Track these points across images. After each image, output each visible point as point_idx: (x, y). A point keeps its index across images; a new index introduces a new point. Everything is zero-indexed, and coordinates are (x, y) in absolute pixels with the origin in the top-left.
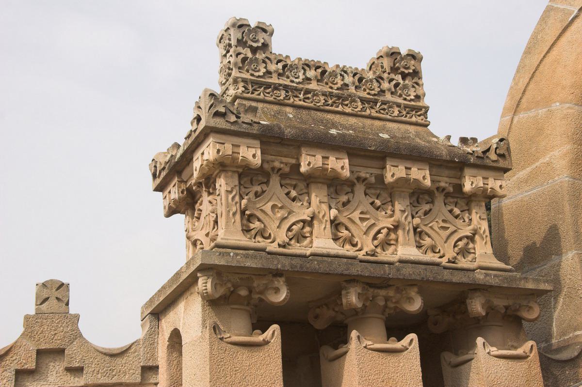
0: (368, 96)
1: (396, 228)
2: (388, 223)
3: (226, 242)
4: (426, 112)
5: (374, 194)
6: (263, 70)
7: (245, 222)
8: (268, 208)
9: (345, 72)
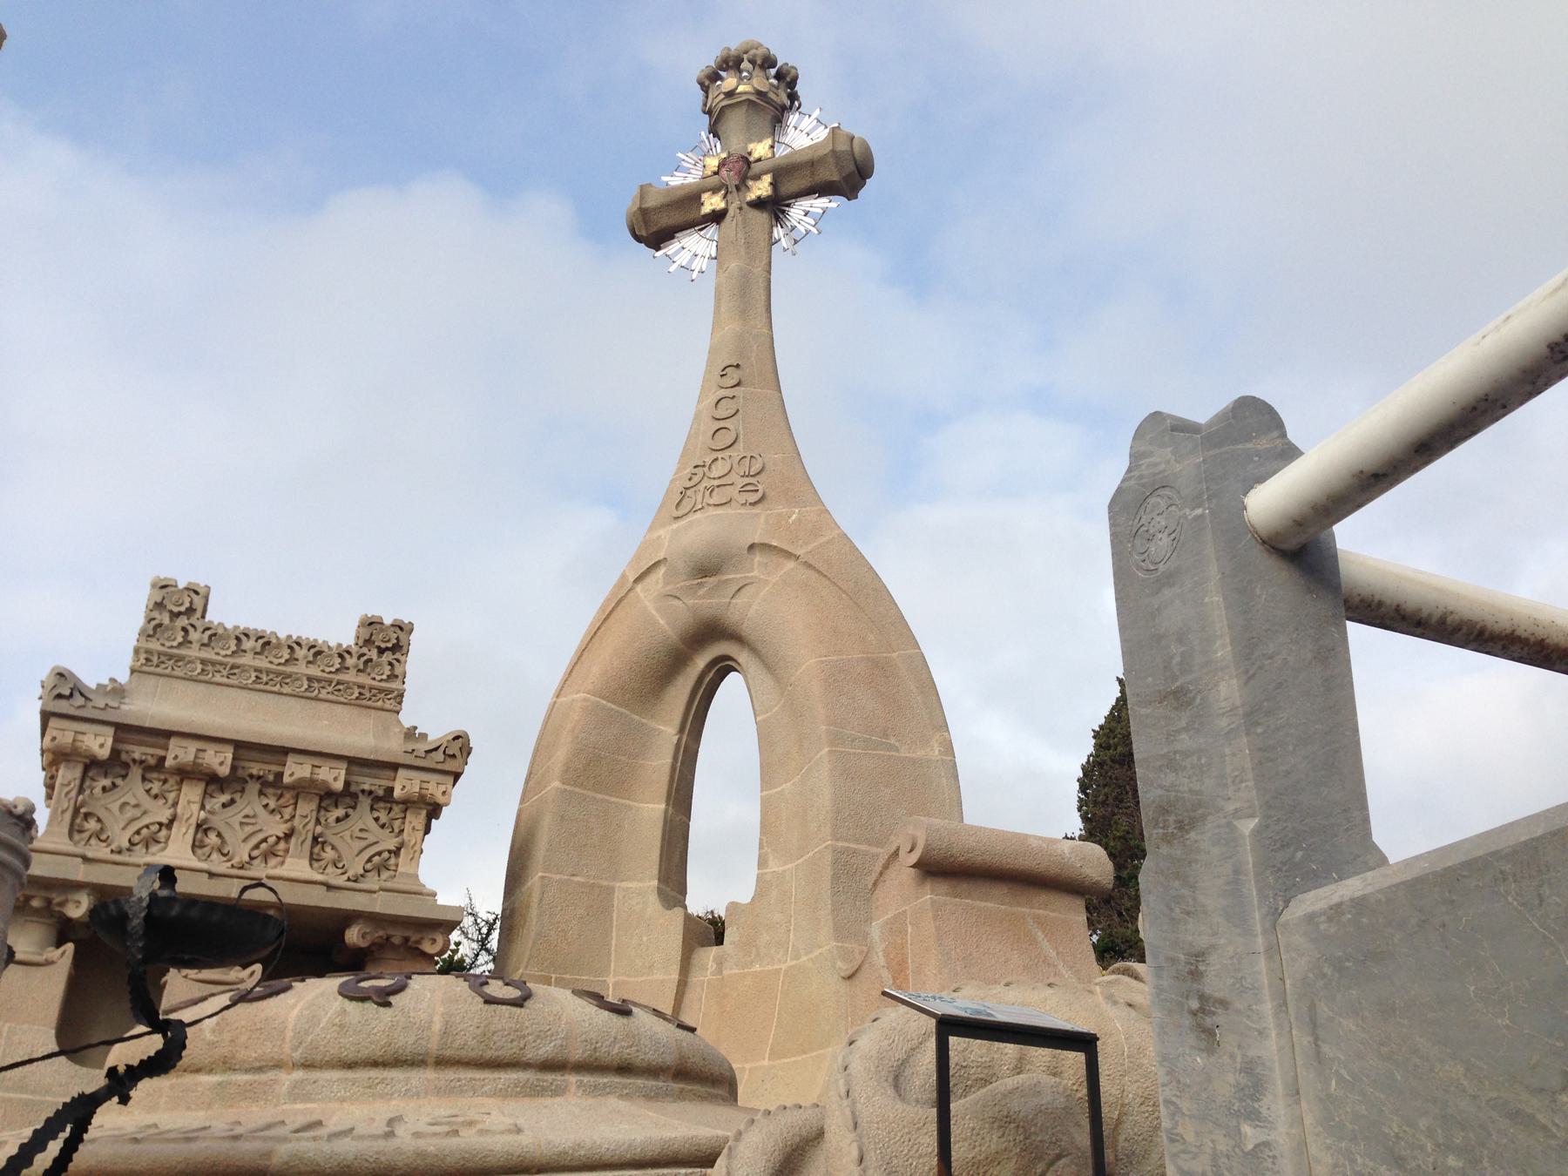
0: (320, 674)
1: (288, 836)
2: (281, 829)
3: (1019, 904)
6: (287, 656)
8: (115, 807)
9: (299, 644)
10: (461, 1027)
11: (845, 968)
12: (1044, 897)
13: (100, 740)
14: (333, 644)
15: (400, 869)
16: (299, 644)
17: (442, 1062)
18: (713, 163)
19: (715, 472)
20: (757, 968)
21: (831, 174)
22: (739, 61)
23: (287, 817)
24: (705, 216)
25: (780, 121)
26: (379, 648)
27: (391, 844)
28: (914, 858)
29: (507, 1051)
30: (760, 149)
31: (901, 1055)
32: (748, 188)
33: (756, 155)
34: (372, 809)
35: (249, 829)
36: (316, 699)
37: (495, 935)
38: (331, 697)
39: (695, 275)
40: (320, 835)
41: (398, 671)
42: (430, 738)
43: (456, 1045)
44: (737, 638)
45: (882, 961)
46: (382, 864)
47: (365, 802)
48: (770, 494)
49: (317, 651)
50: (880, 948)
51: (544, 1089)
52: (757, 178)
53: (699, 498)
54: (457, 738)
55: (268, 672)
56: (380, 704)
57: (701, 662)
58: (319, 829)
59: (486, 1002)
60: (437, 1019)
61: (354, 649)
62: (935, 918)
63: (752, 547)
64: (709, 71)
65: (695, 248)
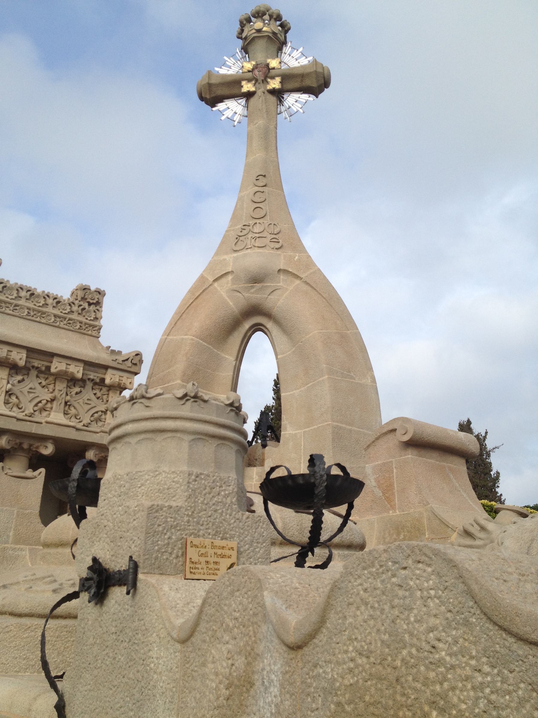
0: (60, 314)
1: (52, 400)
2: (48, 397)
4: (100, 329)
5: (44, 378)
7: (7, 397)
9: (48, 296)
13: (20, 356)
16: (48, 296)
21: (312, 83)
22: (264, 14)
23: (51, 390)
24: (244, 93)
26: (88, 302)
30: (273, 63)
34: (93, 389)
35: (32, 395)
36: (58, 327)
42: (123, 353)
44: (268, 315)
45: (374, 484)
47: (89, 385)
52: (273, 78)
53: (249, 242)
54: (137, 355)
55: (34, 310)
56: (90, 332)
57: (247, 325)
63: (279, 271)
64: (246, 16)
65: (233, 108)
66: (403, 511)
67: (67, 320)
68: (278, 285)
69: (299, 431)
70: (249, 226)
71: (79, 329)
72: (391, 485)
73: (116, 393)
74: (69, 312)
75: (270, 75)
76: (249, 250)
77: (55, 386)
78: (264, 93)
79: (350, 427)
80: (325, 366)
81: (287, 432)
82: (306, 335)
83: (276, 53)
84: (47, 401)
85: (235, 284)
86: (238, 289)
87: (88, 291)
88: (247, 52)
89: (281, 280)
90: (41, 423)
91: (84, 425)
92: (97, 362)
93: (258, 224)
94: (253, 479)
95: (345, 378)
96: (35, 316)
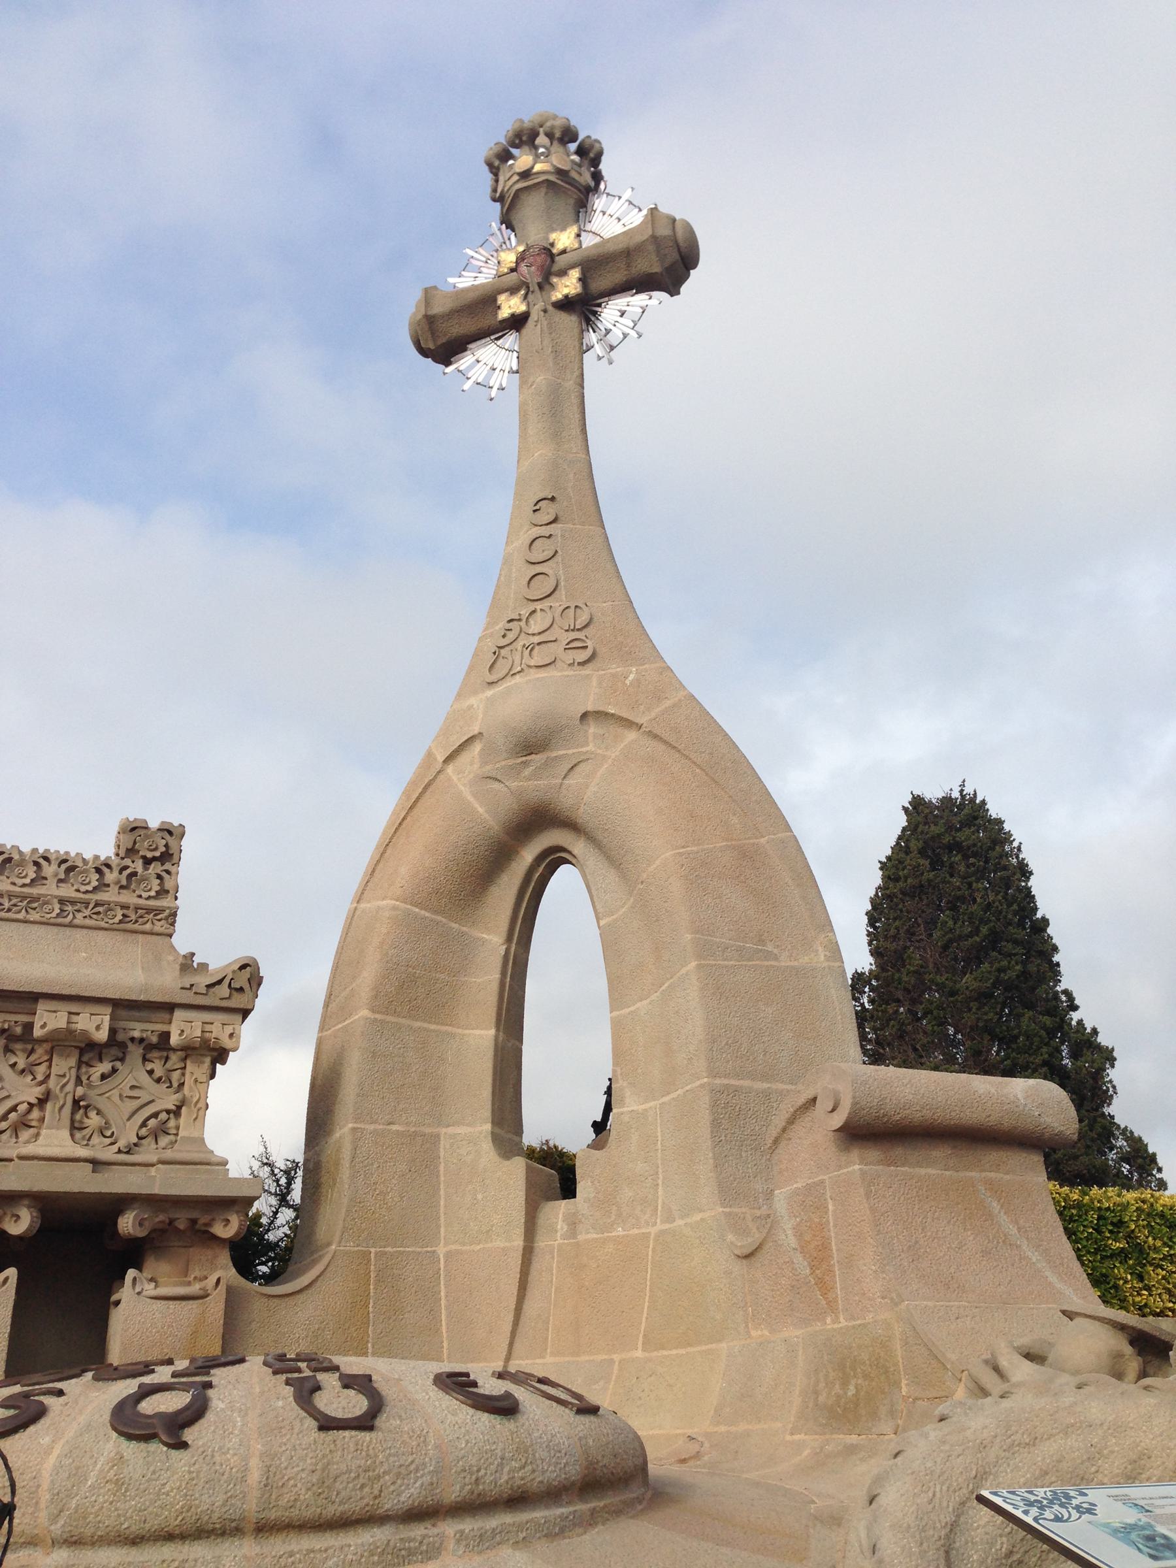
1: (42, 1102)
6: (32, 875)
9: (46, 859)
10: (290, 1472)
11: (746, 1243)
12: (994, 1156)
14: (88, 856)
15: (182, 1133)
16: (46, 859)
17: (264, 1528)
18: (509, 258)
19: (535, 627)
20: (620, 1231)
21: (650, 264)
22: (534, 135)
23: (40, 1078)
24: (504, 321)
25: (585, 206)
26: (144, 857)
27: (170, 1102)
28: (838, 1120)
29: (355, 1506)
30: (564, 239)
31: (947, 1517)
32: (552, 286)
33: (560, 246)
36: (71, 925)
37: (297, 1186)
38: (88, 922)
39: (494, 393)
40: (82, 1098)
41: (168, 885)
43: (283, 1502)
44: (572, 826)
45: (793, 1241)
46: (159, 1128)
47: (135, 1052)
48: (602, 650)
49: (69, 867)
50: (788, 1225)
51: (411, 1553)
52: (563, 273)
53: (517, 658)
54: (243, 967)
56: (148, 927)
57: (528, 855)
58: (80, 1091)
59: (322, 1428)
60: (254, 1463)
61: (115, 861)
62: (868, 1195)
63: (584, 716)
64: (496, 149)
65: (491, 361)
66: (853, 1318)
67: (91, 906)
68: (584, 749)
69: (652, 1104)
70: (520, 620)
71: (121, 922)
72: (825, 1247)
73: (203, 1062)
74: (95, 888)
75: (555, 268)
76: (518, 676)
77: (50, 1067)
78: (545, 311)
79: (766, 1085)
80: (689, 936)
81: (625, 1109)
82: (649, 865)
83: (572, 216)
84: (31, 1105)
85: (486, 763)
86: (494, 775)
87: (142, 832)
88: (510, 226)
89: (591, 738)
90: (11, 1160)
91: (120, 1151)
92: (142, 998)
93: (539, 613)
94: (556, 1231)
95: (749, 960)
96: (15, 909)
